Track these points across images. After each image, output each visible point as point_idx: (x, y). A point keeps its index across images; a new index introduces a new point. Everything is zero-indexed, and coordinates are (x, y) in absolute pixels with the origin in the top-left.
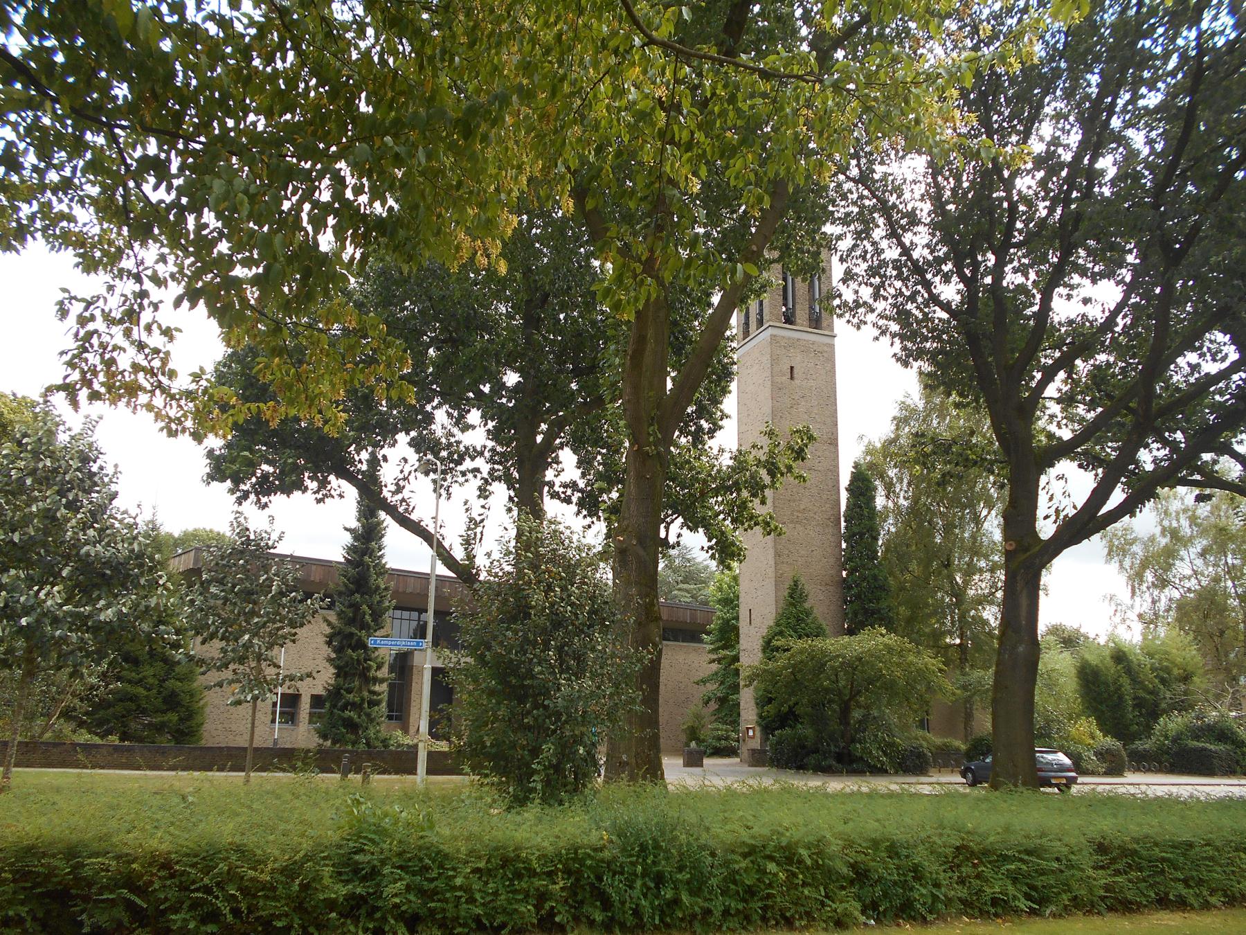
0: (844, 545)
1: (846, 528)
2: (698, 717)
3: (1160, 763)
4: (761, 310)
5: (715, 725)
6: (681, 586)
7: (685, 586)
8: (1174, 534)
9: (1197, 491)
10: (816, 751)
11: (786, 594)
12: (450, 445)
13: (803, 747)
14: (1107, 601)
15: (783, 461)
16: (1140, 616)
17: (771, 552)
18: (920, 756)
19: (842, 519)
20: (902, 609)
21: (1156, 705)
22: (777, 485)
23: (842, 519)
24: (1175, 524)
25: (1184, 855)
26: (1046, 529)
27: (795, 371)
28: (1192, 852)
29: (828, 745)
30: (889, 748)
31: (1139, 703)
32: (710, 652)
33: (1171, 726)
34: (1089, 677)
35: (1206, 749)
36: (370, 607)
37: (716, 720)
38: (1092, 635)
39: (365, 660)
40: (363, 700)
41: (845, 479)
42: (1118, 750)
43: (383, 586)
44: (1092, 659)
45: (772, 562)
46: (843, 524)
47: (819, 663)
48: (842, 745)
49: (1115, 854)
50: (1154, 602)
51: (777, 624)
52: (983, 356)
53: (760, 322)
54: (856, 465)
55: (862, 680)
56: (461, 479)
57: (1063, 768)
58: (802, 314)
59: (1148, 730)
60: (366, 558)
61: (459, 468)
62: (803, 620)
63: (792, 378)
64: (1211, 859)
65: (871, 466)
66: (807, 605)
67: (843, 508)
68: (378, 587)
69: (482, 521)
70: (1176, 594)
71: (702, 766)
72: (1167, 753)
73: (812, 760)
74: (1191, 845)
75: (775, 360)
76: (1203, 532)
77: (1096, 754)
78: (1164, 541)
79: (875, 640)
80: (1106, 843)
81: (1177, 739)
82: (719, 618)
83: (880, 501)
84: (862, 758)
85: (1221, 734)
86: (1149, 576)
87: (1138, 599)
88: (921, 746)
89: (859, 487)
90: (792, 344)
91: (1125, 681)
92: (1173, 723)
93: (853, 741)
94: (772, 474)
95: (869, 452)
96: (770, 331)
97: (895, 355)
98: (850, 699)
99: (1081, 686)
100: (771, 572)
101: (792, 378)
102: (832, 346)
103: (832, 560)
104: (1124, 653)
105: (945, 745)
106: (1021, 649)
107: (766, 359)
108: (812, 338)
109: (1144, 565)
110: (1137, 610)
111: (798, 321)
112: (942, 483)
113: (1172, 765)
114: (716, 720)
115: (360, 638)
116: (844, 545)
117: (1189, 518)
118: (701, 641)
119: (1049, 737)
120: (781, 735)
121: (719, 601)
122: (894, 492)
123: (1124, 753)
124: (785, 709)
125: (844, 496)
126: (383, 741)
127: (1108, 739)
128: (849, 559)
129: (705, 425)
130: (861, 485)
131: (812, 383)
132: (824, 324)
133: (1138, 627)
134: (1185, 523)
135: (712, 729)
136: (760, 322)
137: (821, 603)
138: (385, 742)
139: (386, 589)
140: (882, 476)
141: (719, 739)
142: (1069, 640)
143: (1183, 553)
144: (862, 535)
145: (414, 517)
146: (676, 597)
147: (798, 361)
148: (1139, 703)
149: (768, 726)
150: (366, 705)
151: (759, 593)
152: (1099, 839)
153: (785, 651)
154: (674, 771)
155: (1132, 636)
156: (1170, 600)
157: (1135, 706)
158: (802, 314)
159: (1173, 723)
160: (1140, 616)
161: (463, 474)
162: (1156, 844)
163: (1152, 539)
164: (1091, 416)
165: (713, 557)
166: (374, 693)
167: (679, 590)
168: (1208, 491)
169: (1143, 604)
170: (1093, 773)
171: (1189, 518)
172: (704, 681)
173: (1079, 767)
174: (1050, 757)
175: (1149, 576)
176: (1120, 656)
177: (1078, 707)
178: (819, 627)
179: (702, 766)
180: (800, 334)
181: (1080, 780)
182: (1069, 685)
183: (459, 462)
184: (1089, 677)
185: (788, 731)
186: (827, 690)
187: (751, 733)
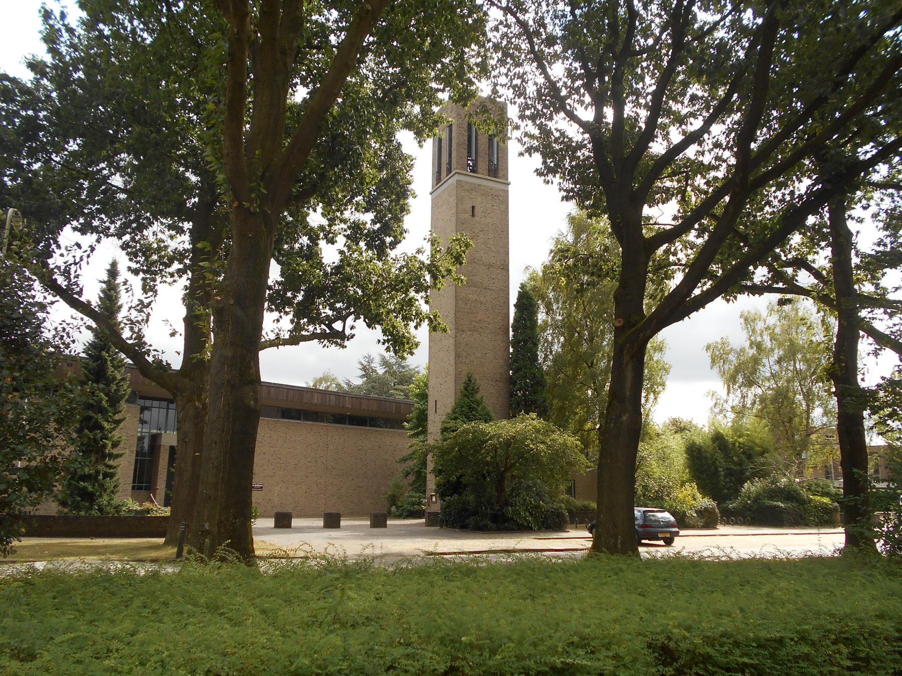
0: (511, 350)
1: (513, 336)
2: (397, 486)
3: (744, 518)
4: (450, 161)
5: (411, 493)
6: (397, 387)
7: (400, 387)
8: (759, 346)
9: (778, 296)
10: (476, 513)
11: (462, 388)
12: (159, 249)
13: (467, 510)
14: (710, 397)
15: (445, 264)
16: (733, 407)
17: (453, 353)
18: (560, 515)
19: (511, 329)
20: (555, 402)
21: (742, 472)
22: (439, 286)
23: (511, 329)
24: (759, 339)
25: (772, 656)
26: (649, 306)
27: (476, 210)
28: (783, 653)
29: (486, 509)
30: (534, 510)
31: (729, 473)
32: (411, 436)
33: (753, 489)
34: (695, 453)
35: (778, 506)
36: (106, 395)
37: (412, 490)
38: (700, 426)
39: (102, 439)
40: (98, 472)
41: (513, 299)
42: (713, 509)
43: (119, 377)
44: (698, 440)
45: (453, 362)
46: (511, 333)
47: (479, 441)
48: (497, 508)
49: (682, 662)
50: (743, 397)
51: (454, 412)
52: (613, 176)
53: (449, 171)
54: (523, 286)
55: (515, 453)
56: (169, 280)
57: (669, 525)
58: (483, 165)
59: (736, 492)
60: (104, 353)
61: (168, 270)
62: (474, 408)
63: (473, 215)
64: (806, 657)
65: (534, 289)
66: (478, 397)
67: (511, 321)
68: (114, 378)
69: (150, 304)
70: (759, 391)
71: (385, 526)
72: (750, 510)
73: (471, 520)
74: (781, 641)
75: (459, 201)
76: (780, 345)
77: (696, 512)
78: (752, 352)
79: (529, 423)
80: (672, 645)
81: (757, 499)
82: (417, 409)
83: (541, 317)
84: (512, 518)
85: (789, 495)
86: (740, 379)
87: (731, 395)
88: (561, 508)
89: (524, 304)
90: (474, 188)
91: (719, 455)
92: (751, 487)
93: (507, 504)
94: (434, 277)
95: (532, 279)
96: (456, 177)
97: (537, 170)
98: (505, 471)
99: (688, 459)
100: (452, 370)
101: (473, 215)
102: (506, 192)
103: (501, 362)
104: (722, 436)
105: (584, 506)
106: (625, 418)
107: (453, 200)
108: (491, 184)
109: (737, 371)
110: (730, 403)
111: (479, 170)
112: (581, 291)
113: (753, 519)
114: (412, 490)
115: (97, 422)
116: (511, 350)
117: (770, 334)
118: (403, 428)
119: (662, 499)
120: (450, 501)
121: (417, 395)
122: (553, 310)
123: (717, 511)
124: (453, 478)
125: (512, 311)
126: (116, 508)
127: (706, 500)
128: (515, 361)
129: (388, 240)
130: (526, 303)
131: (489, 220)
132: (501, 174)
133: (731, 416)
134: (767, 338)
135: (408, 496)
136: (449, 171)
137: (490, 394)
138: (117, 508)
139: (123, 379)
140: (543, 297)
141: (413, 504)
142: (679, 427)
143: (765, 361)
144: (526, 342)
145: (83, 299)
146: (392, 395)
147: (478, 202)
148: (729, 473)
149: (444, 491)
150: (101, 477)
151: (443, 387)
152: (662, 639)
153: (453, 431)
154: (267, 540)
155: (726, 422)
156: (755, 396)
157: (726, 476)
158: (483, 165)
159: (751, 487)
160: (733, 407)
161: (172, 275)
162: (736, 644)
163: (743, 350)
164: (700, 241)
165: (388, 349)
166: (110, 467)
167: (396, 390)
168: (789, 296)
169: (734, 399)
170: (693, 527)
171: (770, 334)
172: (404, 460)
173: (683, 522)
174: (659, 515)
175: (740, 379)
176: (718, 438)
177: (686, 477)
178: (488, 414)
179: (385, 526)
180: (482, 181)
181: (682, 533)
182: (679, 460)
183: (168, 265)
184: (695, 453)
185: (456, 496)
186: (487, 463)
187: (434, 499)
